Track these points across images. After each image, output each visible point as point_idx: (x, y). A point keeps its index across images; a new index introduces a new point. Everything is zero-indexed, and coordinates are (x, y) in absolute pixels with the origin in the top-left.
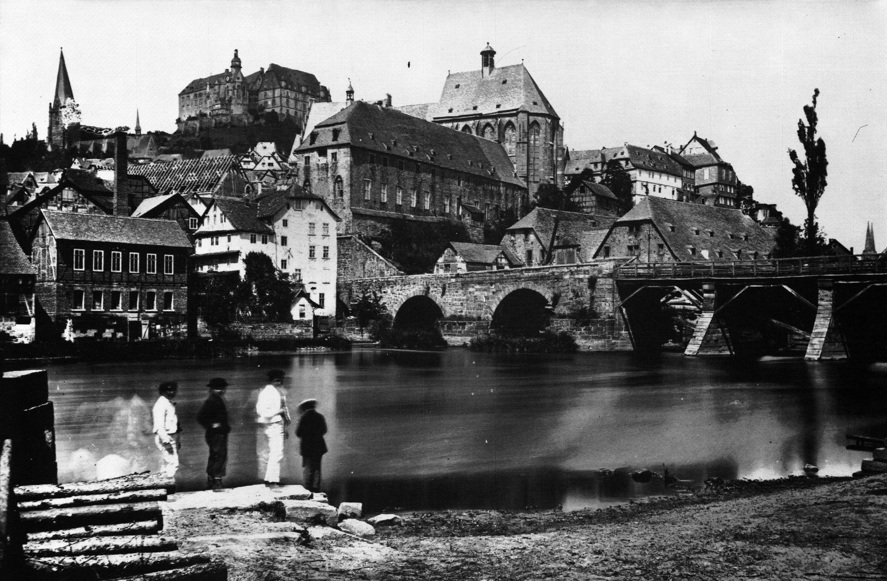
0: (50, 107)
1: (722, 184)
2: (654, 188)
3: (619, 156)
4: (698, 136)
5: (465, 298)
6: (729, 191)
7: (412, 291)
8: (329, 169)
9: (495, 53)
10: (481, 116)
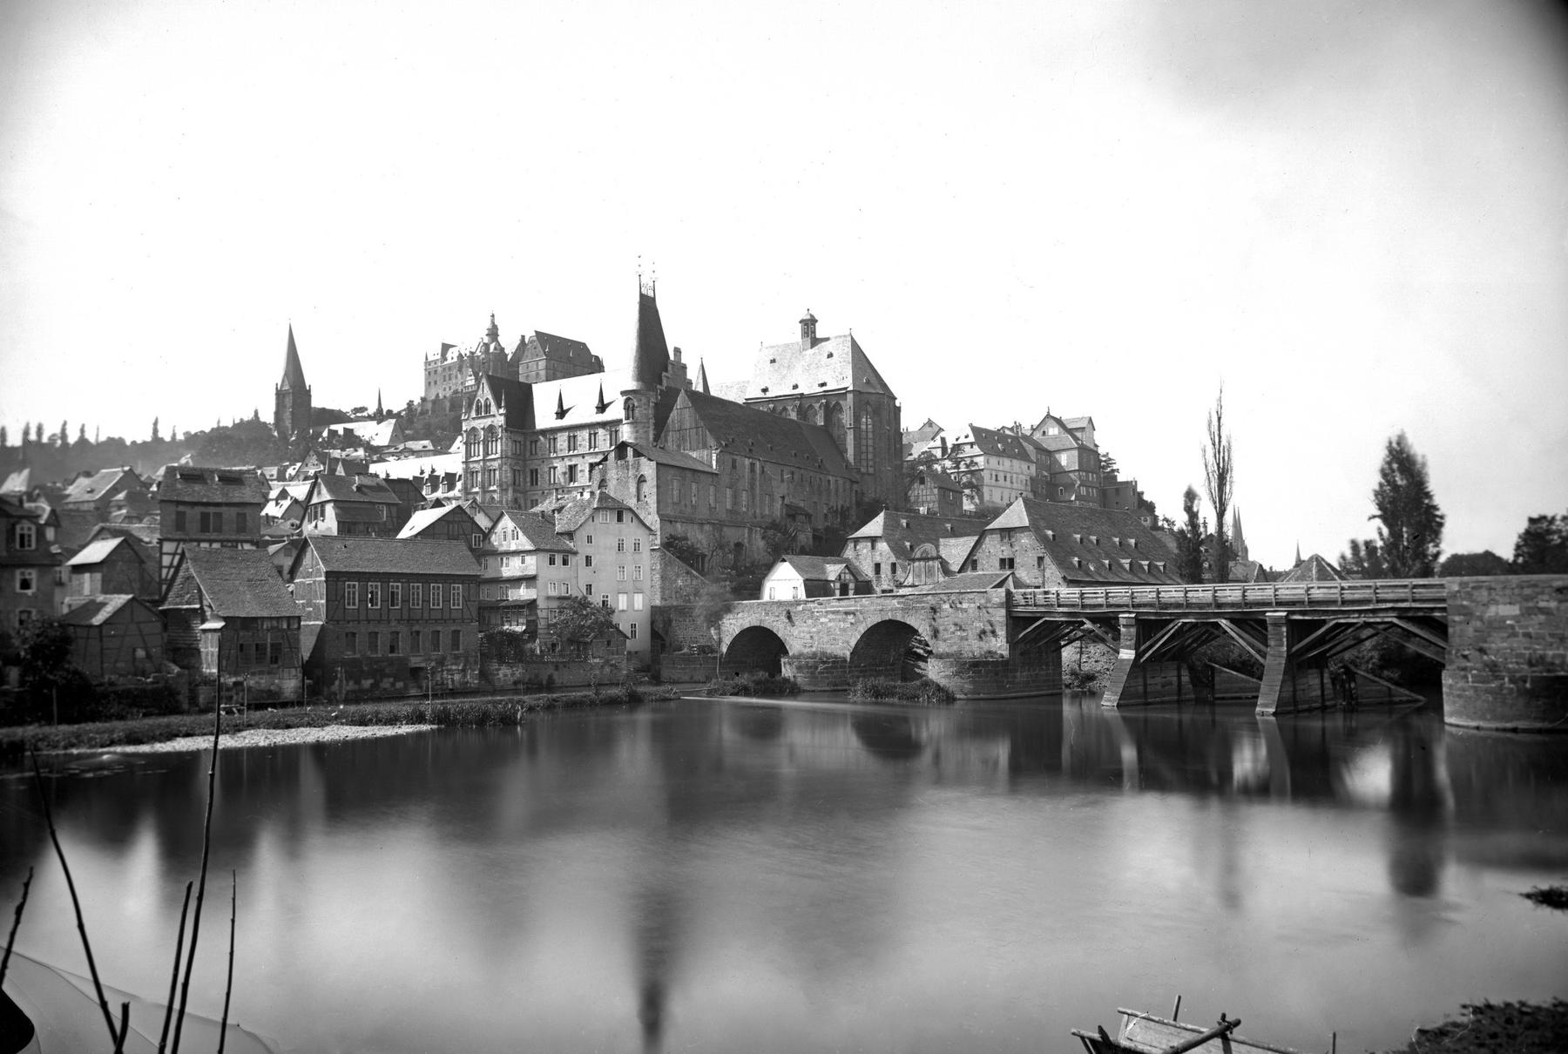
0: (277, 388)
2: (1005, 477)
3: (962, 440)
4: (1051, 414)
6: (1090, 479)
7: (747, 621)
9: (817, 321)
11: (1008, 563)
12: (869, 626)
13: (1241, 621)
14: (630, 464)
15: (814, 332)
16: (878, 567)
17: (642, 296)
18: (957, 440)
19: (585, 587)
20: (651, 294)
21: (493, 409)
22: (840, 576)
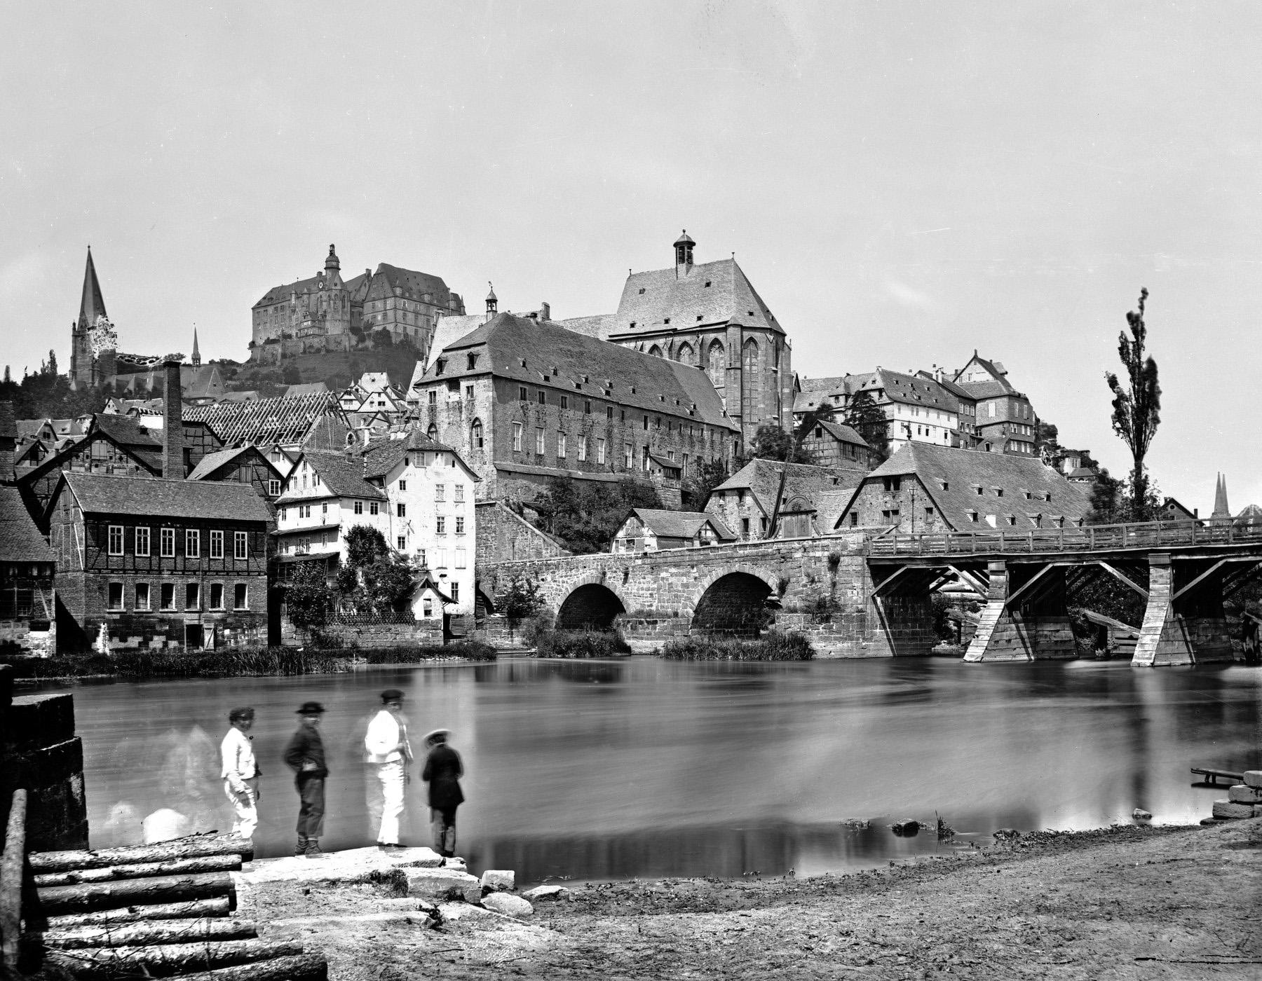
0: (74, 329)
3: (869, 386)
4: (980, 356)
5: (655, 586)
8: (463, 409)
9: (694, 244)
10: (675, 332)
12: (715, 580)
13: (1119, 560)
14: (464, 405)
15: (690, 257)
16: (746, 522)
18: (864, 385)
19: (397, 540)
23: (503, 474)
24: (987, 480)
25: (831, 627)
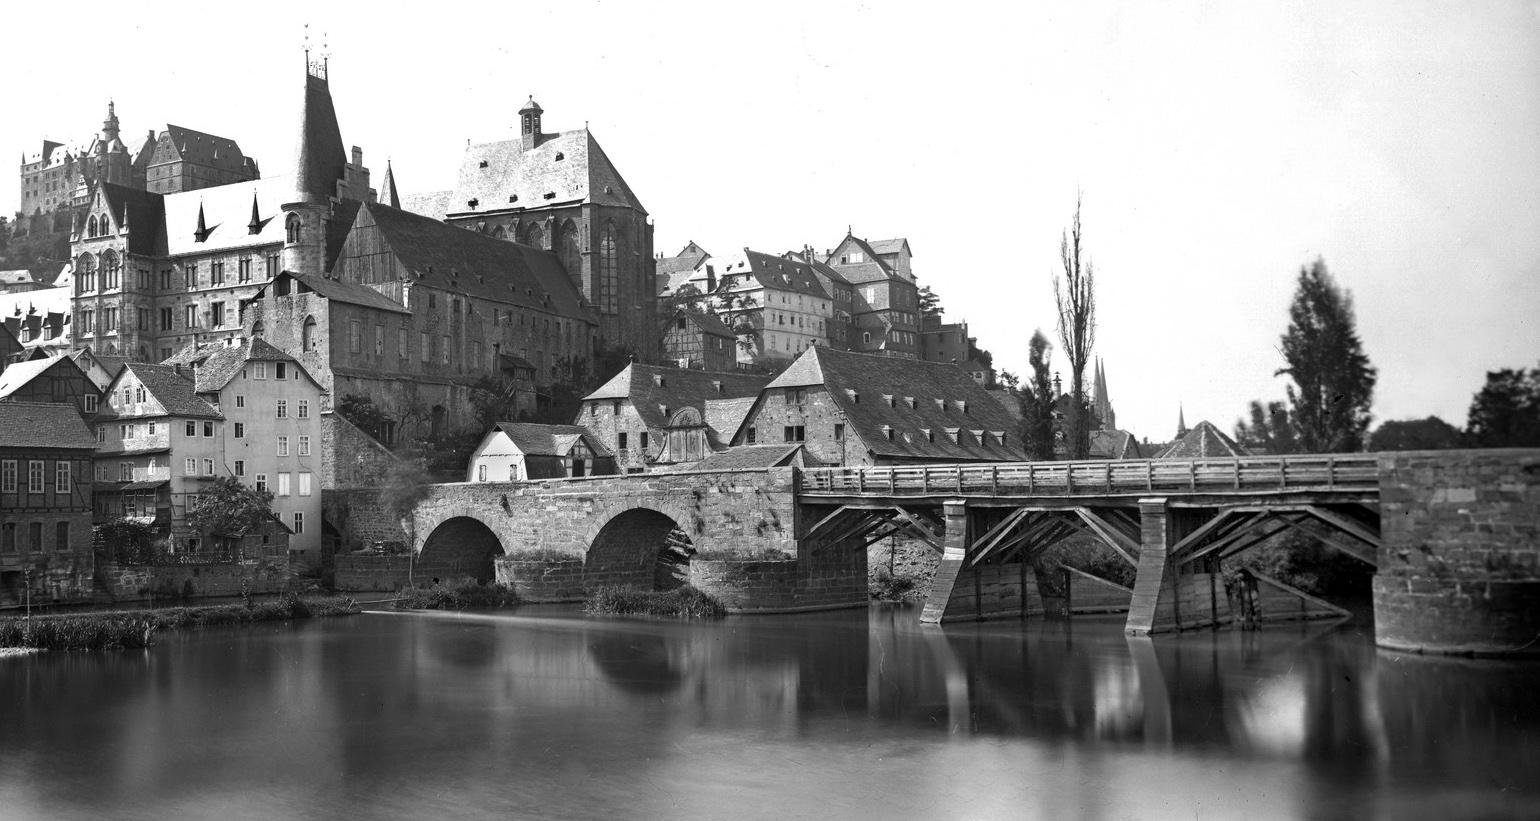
1: (894, 310)
2: (792, 319)
3: (735, 270)
4: (853, 235)
5: (539, 521)
8: (294, 305)
9: (542, 111)
11: (796, 433)
16: (623, 438)
17: (310, 78)
18: (728, 269)
20: (321, 75)
21: (112, 228)
22: (572, 450)
23: (339, 378)
24: (899, 389)
25: (759, 577)
